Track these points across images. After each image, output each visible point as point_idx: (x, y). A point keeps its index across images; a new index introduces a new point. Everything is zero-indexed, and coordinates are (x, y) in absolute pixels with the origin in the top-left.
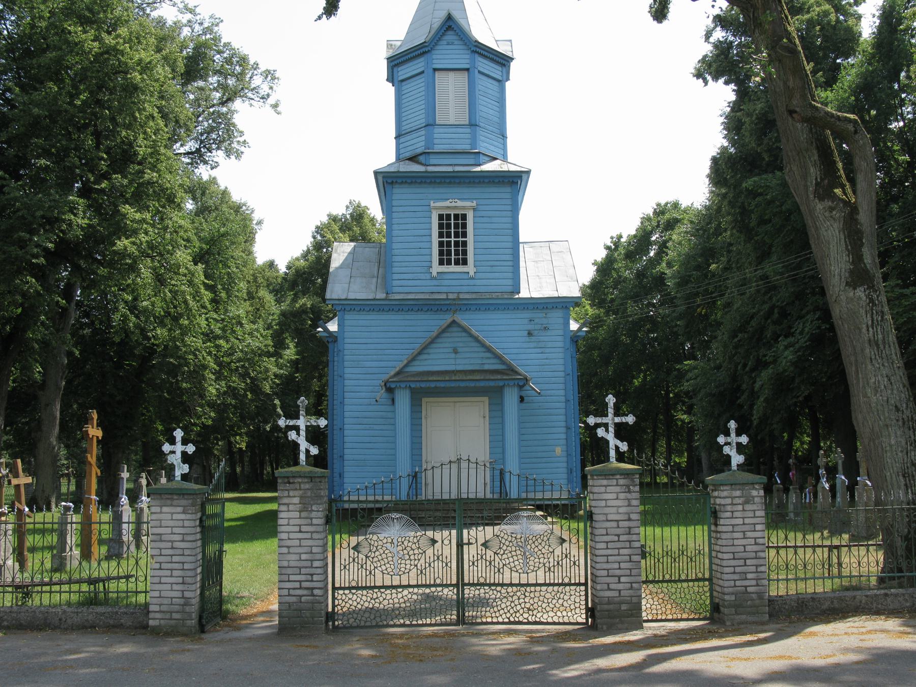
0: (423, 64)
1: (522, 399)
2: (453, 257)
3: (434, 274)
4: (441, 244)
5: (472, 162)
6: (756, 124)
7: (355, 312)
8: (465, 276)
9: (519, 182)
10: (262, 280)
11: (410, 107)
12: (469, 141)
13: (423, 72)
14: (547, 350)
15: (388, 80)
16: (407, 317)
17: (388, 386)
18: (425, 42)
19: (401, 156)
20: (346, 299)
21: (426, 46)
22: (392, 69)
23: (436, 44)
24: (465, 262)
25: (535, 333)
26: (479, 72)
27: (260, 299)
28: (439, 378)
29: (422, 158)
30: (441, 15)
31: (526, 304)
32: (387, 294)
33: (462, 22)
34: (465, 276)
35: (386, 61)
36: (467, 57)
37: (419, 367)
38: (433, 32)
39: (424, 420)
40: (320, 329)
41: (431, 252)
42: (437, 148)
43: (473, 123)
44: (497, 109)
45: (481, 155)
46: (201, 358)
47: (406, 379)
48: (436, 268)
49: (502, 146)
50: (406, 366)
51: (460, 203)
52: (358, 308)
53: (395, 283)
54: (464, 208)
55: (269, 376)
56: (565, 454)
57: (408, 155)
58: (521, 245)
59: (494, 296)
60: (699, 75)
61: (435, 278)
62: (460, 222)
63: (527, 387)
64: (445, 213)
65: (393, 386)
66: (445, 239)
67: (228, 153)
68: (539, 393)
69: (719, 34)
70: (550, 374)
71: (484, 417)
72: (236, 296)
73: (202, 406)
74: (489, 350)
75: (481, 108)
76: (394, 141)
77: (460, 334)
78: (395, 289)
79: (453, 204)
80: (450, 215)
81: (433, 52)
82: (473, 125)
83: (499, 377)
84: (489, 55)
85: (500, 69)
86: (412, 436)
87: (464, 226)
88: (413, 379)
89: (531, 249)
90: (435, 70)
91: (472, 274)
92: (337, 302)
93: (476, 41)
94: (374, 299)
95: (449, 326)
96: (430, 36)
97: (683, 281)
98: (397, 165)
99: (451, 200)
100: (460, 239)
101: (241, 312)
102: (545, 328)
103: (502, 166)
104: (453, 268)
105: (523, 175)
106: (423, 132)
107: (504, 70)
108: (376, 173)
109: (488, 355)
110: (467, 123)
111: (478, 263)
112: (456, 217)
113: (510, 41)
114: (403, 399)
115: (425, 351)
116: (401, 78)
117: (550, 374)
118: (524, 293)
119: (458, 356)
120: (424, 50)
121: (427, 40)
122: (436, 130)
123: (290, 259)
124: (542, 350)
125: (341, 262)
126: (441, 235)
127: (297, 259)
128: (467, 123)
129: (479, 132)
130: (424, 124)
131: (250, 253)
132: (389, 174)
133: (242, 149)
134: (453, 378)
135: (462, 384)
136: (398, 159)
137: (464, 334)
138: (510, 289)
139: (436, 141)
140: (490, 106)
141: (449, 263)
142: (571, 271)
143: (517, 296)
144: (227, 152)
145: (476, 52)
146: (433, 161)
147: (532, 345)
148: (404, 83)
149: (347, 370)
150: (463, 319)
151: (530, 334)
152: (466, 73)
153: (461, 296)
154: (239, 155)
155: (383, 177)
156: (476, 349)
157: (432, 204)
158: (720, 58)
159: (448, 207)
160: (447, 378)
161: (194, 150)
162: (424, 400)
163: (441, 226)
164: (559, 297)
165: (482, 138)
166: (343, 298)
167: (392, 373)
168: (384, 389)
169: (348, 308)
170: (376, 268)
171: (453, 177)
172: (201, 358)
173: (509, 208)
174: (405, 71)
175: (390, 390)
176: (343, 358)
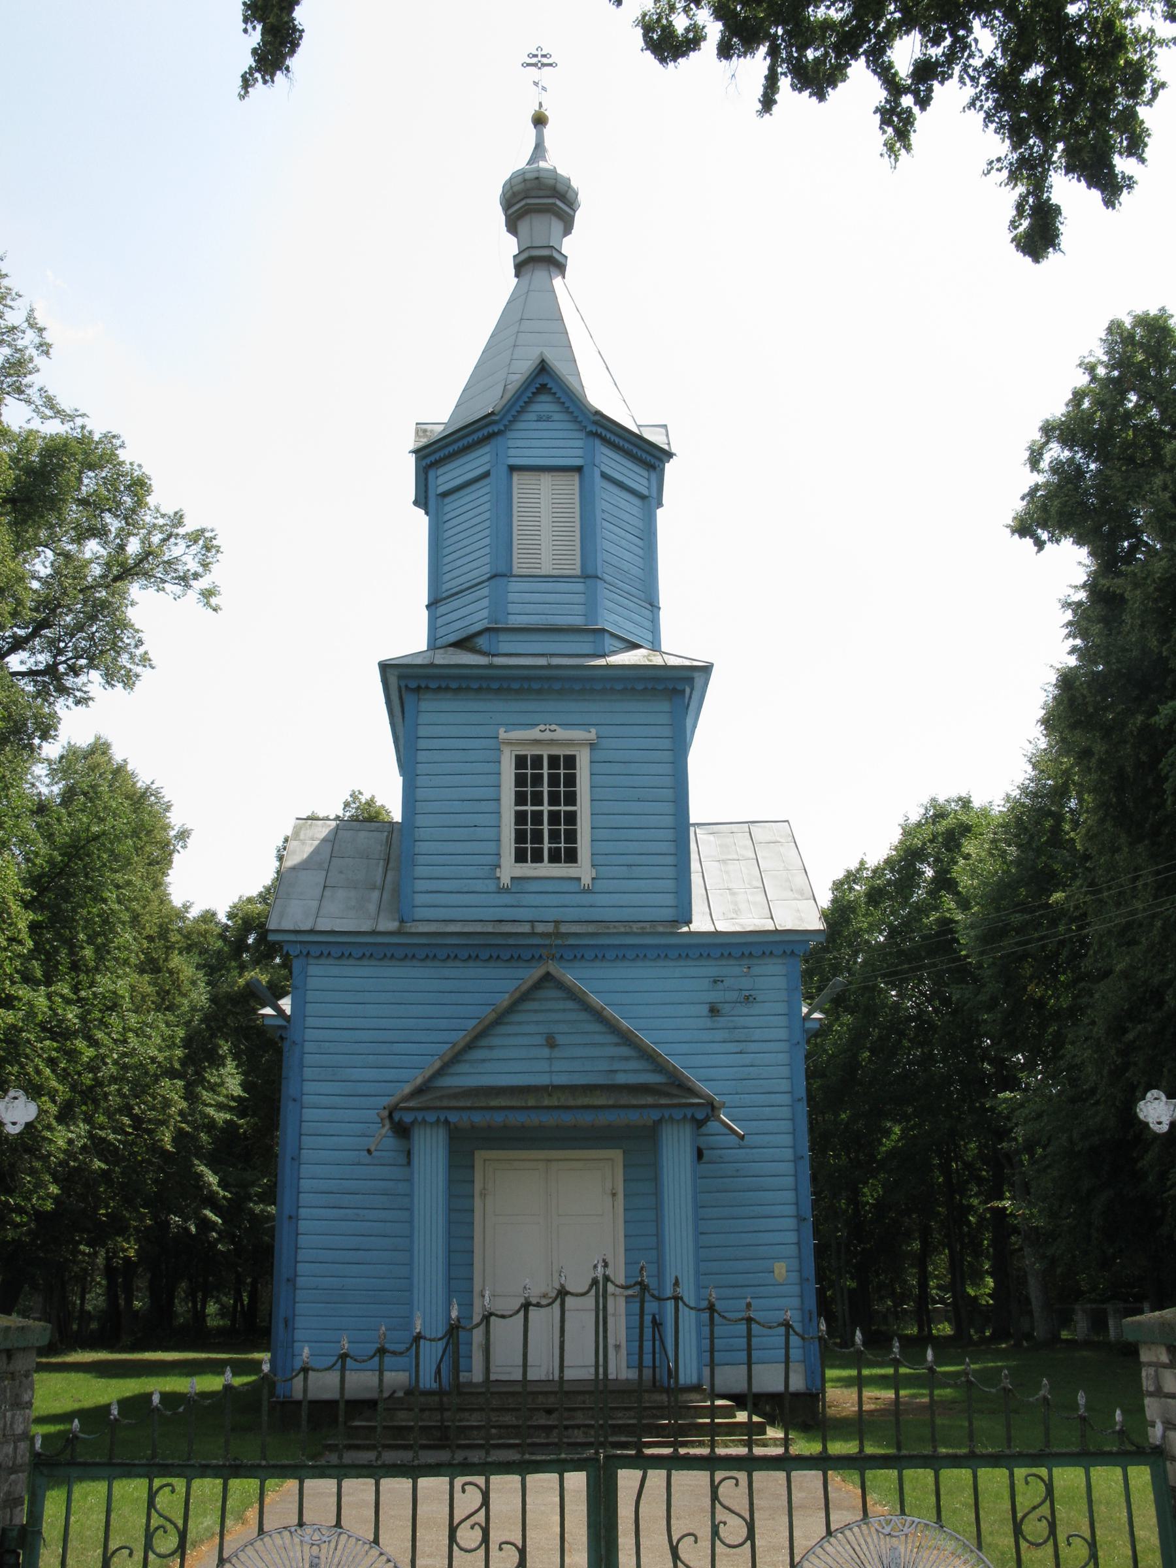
0: (486, 458)
1: (700, 1154)
2: (546, 846)
3: (505, 880)
4: (520, 818)
5: (587, 648)
6: (1156, 600)
7: (331, 961)
8: (572, 887)
9: (688, 690)
10: (179, 937)
11: (461, 545)
12: (580, 609)
13: (486, 475)
14: (753, 1047)
16: (446, 972)
17: (396, 1118)
18: (492, 413)
19: (439, 643)
20: (312, 932)
21: (495, 422)
22: (426, 474)
23: (515, 420)
25: (726, 1008)
26: (604, 476)
27: (171, 972)
28: (514, 1103)
29: (482, 642)
30: (524, 367)
31: (703, 945)
32: (402, 921)
33: (571, 380)
34: (572, 887)
35: (412, 459)
36: (579, 443)
37: (467, 1077)
38: (508, 395)
39: (478, 1202)
40: (268, 1011)
41: (499, 833)
42: (516, 621)
43: (590, 572)
44: (640, 552)
45: (607, 636)
46: (30, 1070)
47: (438, 1104)
48: (509, 869)
49: (647, 624)
50: (440, 1072)
51: (561, 734)
52: (336, 951)
53: (420, 899)
54: (570, 743)
55: (170, 1116)
56: (794, 1276)
57: (453, 638)
58: (692, 829)
59: (635, 928)
60: (1023, 528)
62: (562, 771)
63: (713, 1126)
64: (529, 753)
65: (408, 1118)
66: (529, 808)
67: (109, 678)
68: (742, 1137)
69: (1056, 452)
70: (762, 1099)
71: (614, 1195)
72: (116, 959)
73: (32, 1172)
74: (626, 1039)
75: (607, 545)
76: (426, 613)
77: (561, 1005)
78: (420, 913)
79: (548, 735)
80: (540, 757)
81: (510, 434)
82: (589, 576)
83: (650, 1100)
84: (622, 443)
85: (645, 474)
86: (450, 1236)
87: (571, 780)
88: (453, 1103)
89: (711, 838)
90: (513, 469)
91: (586, 880)
92: (292, 938)
93: (598, 413)
94: (373, 933)
95: (539, 985)
96: (504, 401)
97: (991, 935)
98: (429, 653)
99: (542, 727)
100: (563, 808)
101: (122, 987)
102: (747, 998)
103: (652, 658)
104: (546, 869)
105: (696, 675)
106: (485, 592)
107: (654, 477)
109: (625, 1051)
110: (578, 572)
111: (600, 860)
112: (554, 761)
113: (665, 426)
115: (484, 1042)
116: (441, 490)
117: (762, 1099)
118: (700, 923)
119: (556, 1053)
120: (490, 429)
121: (498, 409)
122: (514, 586)
123: (236, 900)
124: (741, 1046)
125: (305, 856)
126: (520, 799)
127: (250, 900)
128: (578, 572)
129: (603, 592)
130: (488, 575)
131: (157, 885)
132: (410, 671)
133: (138, 669)
134: (546, 1103)
135: (567, 1118)
136: (434, 643)
137: (570, 1005)
138: (668, 914)
139: (512, 608)
140: (623, 543)
141: (537, 857)
142: (800, 879)
143: (685, 929)
144: (106, 675)
145: (596, 435)
146: (505, 648)
147: (720, 1035)
148: (447, 500)
149: (309, 1087)
150: (569, 975)
151: (714, 1011)
152: (576, 477)
153: (564, 929)
154: (129, 680)
155: (400, 677)
156: (599, 1039)
157: (502, 734)
158: (1065, 490)
159: (537, 742)
160: (531, 1103)
161: (41, 667)
162: (480, 1156)
163: (520, 780)
164: (777, 931)
165: (610, 605)
166: (306, 926)
167: (407, 1089)
168: (388, 1126)
169: (314, 951)
170: (380, 870)
171: (549, 679)
172: (30, 1070)
173: (667, 743)
174: (449, 476)
175: (402, 1131)
176: (301, 1059)
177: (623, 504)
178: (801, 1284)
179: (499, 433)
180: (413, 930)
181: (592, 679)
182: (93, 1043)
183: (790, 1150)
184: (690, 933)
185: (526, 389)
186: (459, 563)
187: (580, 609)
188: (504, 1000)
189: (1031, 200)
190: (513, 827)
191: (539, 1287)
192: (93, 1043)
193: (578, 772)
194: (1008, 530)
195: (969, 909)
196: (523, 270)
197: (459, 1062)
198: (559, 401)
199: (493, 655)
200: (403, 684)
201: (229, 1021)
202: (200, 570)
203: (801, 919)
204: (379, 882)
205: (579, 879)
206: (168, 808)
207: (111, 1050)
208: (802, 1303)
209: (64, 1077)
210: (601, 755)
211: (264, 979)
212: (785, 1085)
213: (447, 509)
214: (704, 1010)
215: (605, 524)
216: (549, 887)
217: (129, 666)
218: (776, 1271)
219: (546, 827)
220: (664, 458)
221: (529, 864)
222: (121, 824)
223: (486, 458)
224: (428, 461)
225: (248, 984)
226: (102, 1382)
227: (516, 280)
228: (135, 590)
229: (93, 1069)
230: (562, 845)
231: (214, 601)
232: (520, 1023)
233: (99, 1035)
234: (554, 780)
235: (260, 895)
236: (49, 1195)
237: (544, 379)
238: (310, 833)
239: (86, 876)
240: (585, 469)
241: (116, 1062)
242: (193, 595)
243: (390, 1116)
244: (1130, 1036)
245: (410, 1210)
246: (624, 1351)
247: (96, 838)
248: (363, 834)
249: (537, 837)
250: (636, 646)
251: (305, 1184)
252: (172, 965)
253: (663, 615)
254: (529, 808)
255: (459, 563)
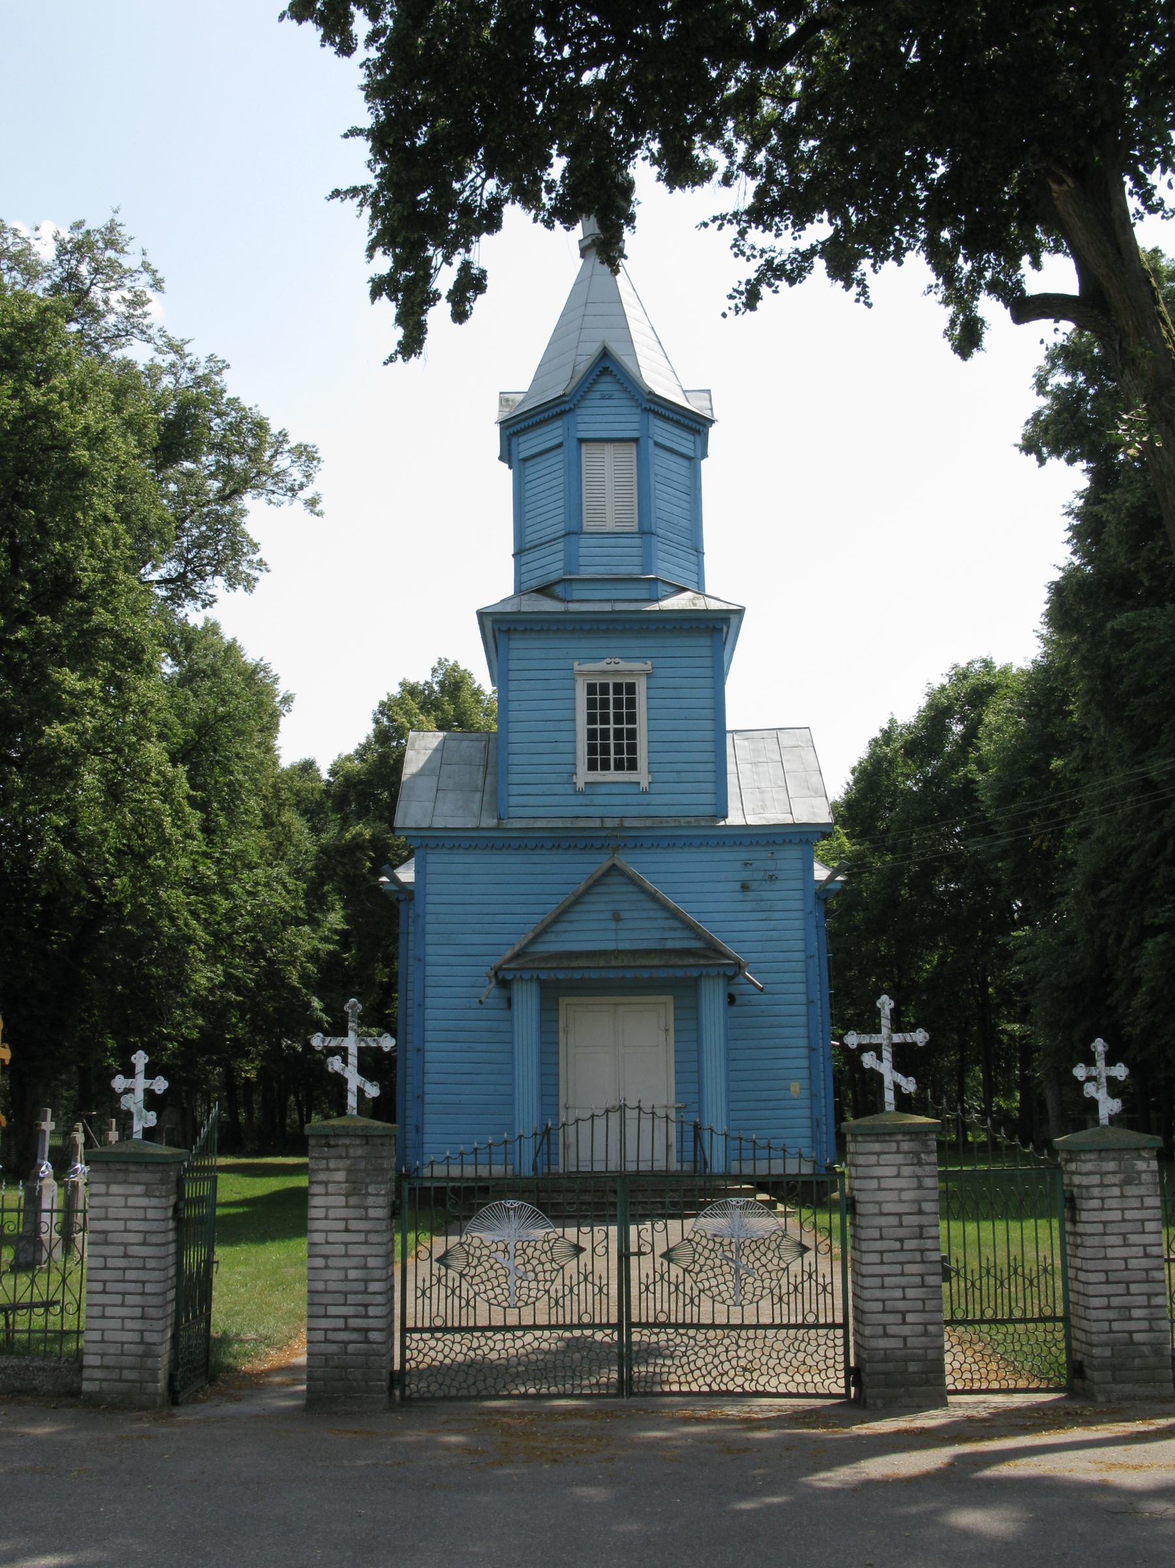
0: (560, 431)
1: (731, 999)
2: (612, 756)
3: (580, 785)
4: (592, 734)
5: (644, 594)
6: (1126, 525)
8: (633, 789)
10: (289, 795)
12: (638, 560)
13: (560, 445)
14: (776, 915)
15: (501, 458)
16: (536, 858)
17: (500, 975)
18: (564, 395)
19: (524, 586)
20: (430, 828)
21: (566, 402)
23: (583, 398)
24: (633, 765)
25: (754, 886)
26: (657, 444)
27: (282, 825)
30: (591, 350)
31: (737, 835)
32: (500, 819)
33: (626, 360)
34: (633, 789)
35: (497, 429)
37: (554, 944)
39: (561, 1034)
40: (384, 879)
42: (586, 572)
45: (660, 584)
47: (531, 965)
48: (583, 776)
49: (694, 568)
50: (533, 941)
51: (624, 665)
53: (513, 800)
54: (631, 673)
55: (297, 957)
56: (806, 1093)
57: (535, 583)
58: (729, 737)
59: (683, 822)
60: (1029, 446)
61: (581, 793)
63: (740, 979)
64: (598, 682)
65: (509, 976)
66: (598, 726)
67: (232, 582)
68: (762, 989)
69: (1060, 379)
71: (667, 1030)
74: (674, 914)
75: (660, 504)
76: (512, 560)
79: (613, 667)
81: (579, 411)
82: (645, 533)
83: (692, 961)
85: (691, 438)
87: (632, 703)
88: (543, 965)
89: (746, 743)
90: (581, 441)
91: (644, 784)
94: (478, 829)
97: (1007, 794)
98: (516, 600)
99: (608, 660)
100: (625, 726)
102: (771, 877)
103: (696, 602)
104: (612, 775)
105: (732, 616)
106: (561, 546)
108: (481, 615)
109: (673, 923)
110: (635, 529)
111: (655, 767)
112: (618, 688)
113: (708, 391)
114: (527, 1001)
116: (522, 456)
118: (734, 818)
119: (621, 925)
120: (562, 408)
123: (336, 758)
125: (421, 764)
126: (591, 719)
127: (349, 758)
131: (269, 749)
133: (256, 573)
134: (613, 963)
136: (519, 590)
137: (631, 888)
138: (709, 810)
140: (674, 500)
141: (605, 766)
142: (815, 779)
143: (722, 823)
146: (577, 595)
147: (749, 906)
148: (528, 464)
151: (745, 887)
152: (634, 446)
153: (627, 823)
154: (250, 584)
155: (494, 622)
156: (652, 914)
157: (576, 667)
160: (602, 964)
162: (563, 1001)
163: (591, 704)
165: (661, 554)
167: (508, 954)
170: (481, 775)
173: (708, 672)
174: (529, 444)
177: (674, 467)
178: (811, 1099)
179: (570, 410)
180: (509, 826)
181: (649, 621)
182: (229, 895)
183: (804, 996)
184: (726, 826)
185: (591, 373)
186: (538, 519)
187: (638, 560)
188: (582, 882)
189: (961, 317)
190: (586, 742)
191: (612, 1102)
192: (229, 895)
193: (637, 696)
194: (1017, 449)
195: (987, 771)
196: (587, 253)
197: (547, 933)
198: (618, 382)
199: (569, 601)
200: (496, 627)
201: (338, 870)
202: (304, 480)
203: (814, 814)
204: (480, 783)
205: (638, 783)
206: (276, 680)
207: (246, 902)
208: (812, 1113)
209: (206, 924)
210: (656, 682)
211: (367, 834)
212: (800, 945)
213: (528, 471)
214: (738, 886)
215: (659, 486)
216: (615, 789)
217: (248, 571)
218: (792, 1089)
219: (612, 742)
220: (708, 424)
221: (599, 772)
222: (245, 706)
223: (560, 431)
224: (511, 431)
225: (354, 838)
226: (248, 1180)
227: (582, 261)
228: (248, 500)
229: (230, 920)
230: (625, 756)
231: (318, 508)
232: (593, 903)
233: (235, 887)
234: (618, 704)
235: (357, 752)
236: (195, 1026)
237: (607, 364)
238: (423, 743)
239: (215, 751)
240: (641, 440)
241: (250, 913)
242: (298, 504)
243: (496, 975)
244: (1103, 894)
245: (511, 1043)
246: (561, 1104)
247: (222, 719)
248: (466, 743)
249: (605, 750)
250: (684, 590)
251: (429, 1024)
252: (283, 819)
253: (707, 559)
254: (598, 726)
255: (538, 519)
